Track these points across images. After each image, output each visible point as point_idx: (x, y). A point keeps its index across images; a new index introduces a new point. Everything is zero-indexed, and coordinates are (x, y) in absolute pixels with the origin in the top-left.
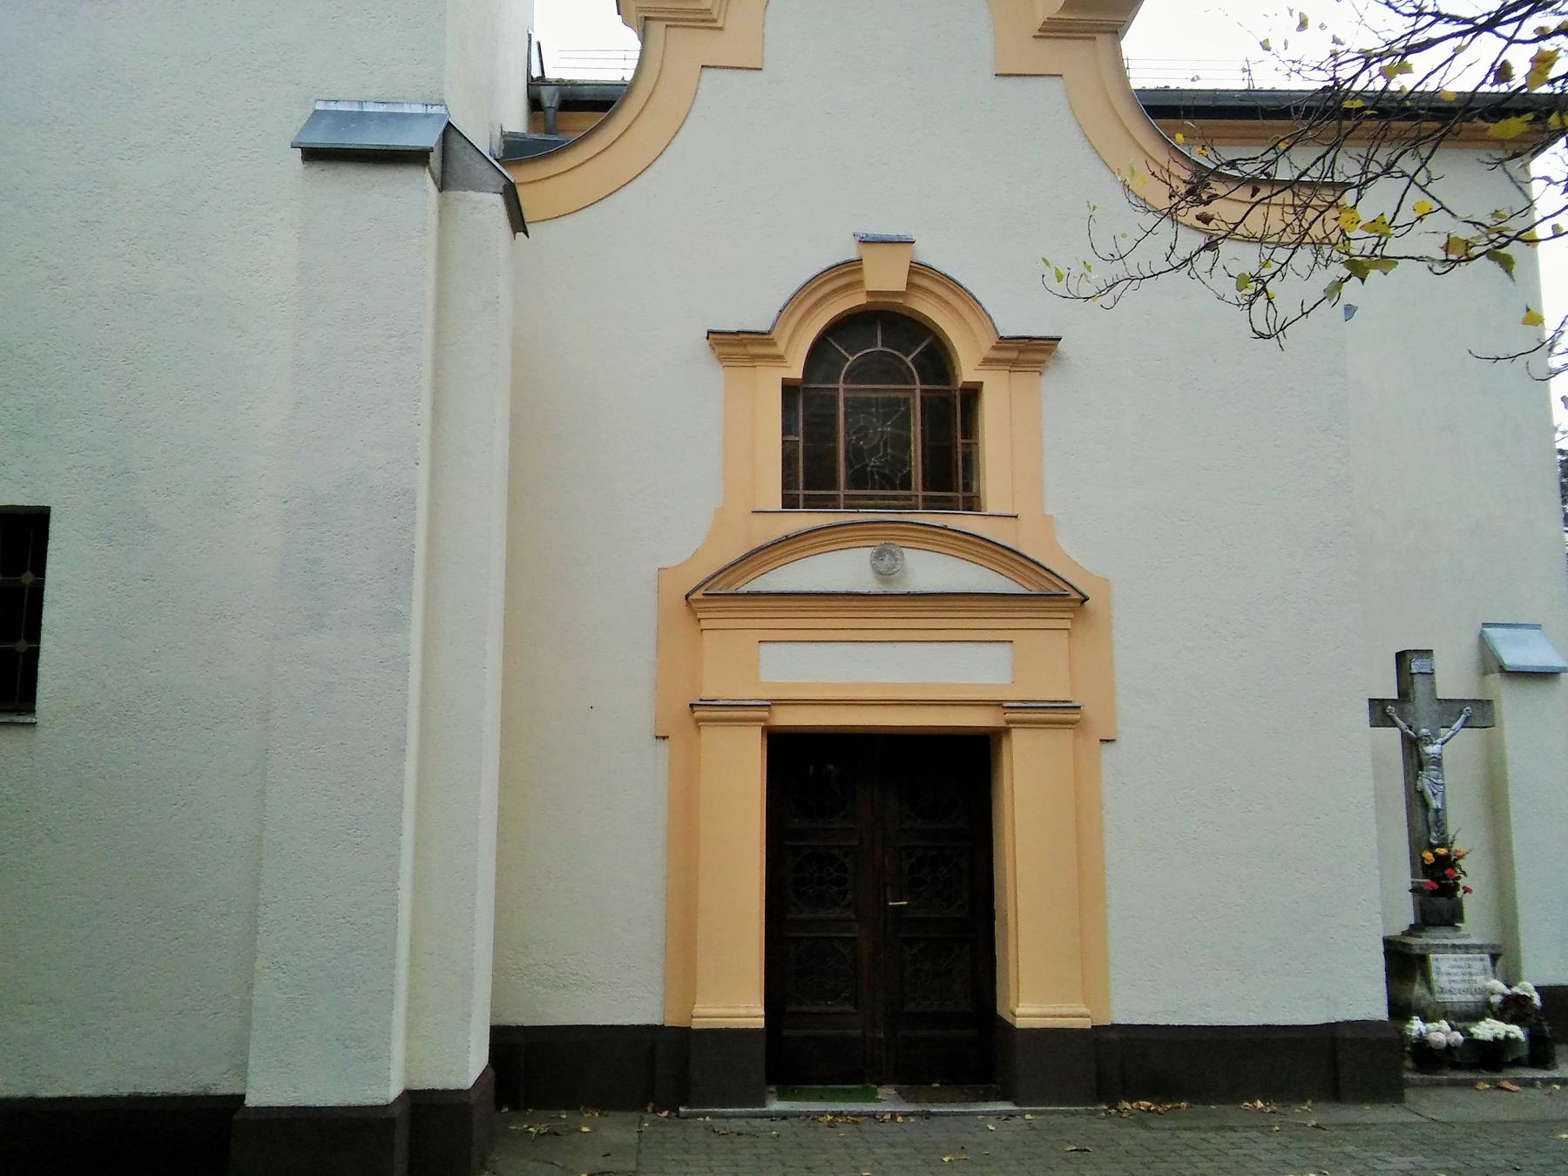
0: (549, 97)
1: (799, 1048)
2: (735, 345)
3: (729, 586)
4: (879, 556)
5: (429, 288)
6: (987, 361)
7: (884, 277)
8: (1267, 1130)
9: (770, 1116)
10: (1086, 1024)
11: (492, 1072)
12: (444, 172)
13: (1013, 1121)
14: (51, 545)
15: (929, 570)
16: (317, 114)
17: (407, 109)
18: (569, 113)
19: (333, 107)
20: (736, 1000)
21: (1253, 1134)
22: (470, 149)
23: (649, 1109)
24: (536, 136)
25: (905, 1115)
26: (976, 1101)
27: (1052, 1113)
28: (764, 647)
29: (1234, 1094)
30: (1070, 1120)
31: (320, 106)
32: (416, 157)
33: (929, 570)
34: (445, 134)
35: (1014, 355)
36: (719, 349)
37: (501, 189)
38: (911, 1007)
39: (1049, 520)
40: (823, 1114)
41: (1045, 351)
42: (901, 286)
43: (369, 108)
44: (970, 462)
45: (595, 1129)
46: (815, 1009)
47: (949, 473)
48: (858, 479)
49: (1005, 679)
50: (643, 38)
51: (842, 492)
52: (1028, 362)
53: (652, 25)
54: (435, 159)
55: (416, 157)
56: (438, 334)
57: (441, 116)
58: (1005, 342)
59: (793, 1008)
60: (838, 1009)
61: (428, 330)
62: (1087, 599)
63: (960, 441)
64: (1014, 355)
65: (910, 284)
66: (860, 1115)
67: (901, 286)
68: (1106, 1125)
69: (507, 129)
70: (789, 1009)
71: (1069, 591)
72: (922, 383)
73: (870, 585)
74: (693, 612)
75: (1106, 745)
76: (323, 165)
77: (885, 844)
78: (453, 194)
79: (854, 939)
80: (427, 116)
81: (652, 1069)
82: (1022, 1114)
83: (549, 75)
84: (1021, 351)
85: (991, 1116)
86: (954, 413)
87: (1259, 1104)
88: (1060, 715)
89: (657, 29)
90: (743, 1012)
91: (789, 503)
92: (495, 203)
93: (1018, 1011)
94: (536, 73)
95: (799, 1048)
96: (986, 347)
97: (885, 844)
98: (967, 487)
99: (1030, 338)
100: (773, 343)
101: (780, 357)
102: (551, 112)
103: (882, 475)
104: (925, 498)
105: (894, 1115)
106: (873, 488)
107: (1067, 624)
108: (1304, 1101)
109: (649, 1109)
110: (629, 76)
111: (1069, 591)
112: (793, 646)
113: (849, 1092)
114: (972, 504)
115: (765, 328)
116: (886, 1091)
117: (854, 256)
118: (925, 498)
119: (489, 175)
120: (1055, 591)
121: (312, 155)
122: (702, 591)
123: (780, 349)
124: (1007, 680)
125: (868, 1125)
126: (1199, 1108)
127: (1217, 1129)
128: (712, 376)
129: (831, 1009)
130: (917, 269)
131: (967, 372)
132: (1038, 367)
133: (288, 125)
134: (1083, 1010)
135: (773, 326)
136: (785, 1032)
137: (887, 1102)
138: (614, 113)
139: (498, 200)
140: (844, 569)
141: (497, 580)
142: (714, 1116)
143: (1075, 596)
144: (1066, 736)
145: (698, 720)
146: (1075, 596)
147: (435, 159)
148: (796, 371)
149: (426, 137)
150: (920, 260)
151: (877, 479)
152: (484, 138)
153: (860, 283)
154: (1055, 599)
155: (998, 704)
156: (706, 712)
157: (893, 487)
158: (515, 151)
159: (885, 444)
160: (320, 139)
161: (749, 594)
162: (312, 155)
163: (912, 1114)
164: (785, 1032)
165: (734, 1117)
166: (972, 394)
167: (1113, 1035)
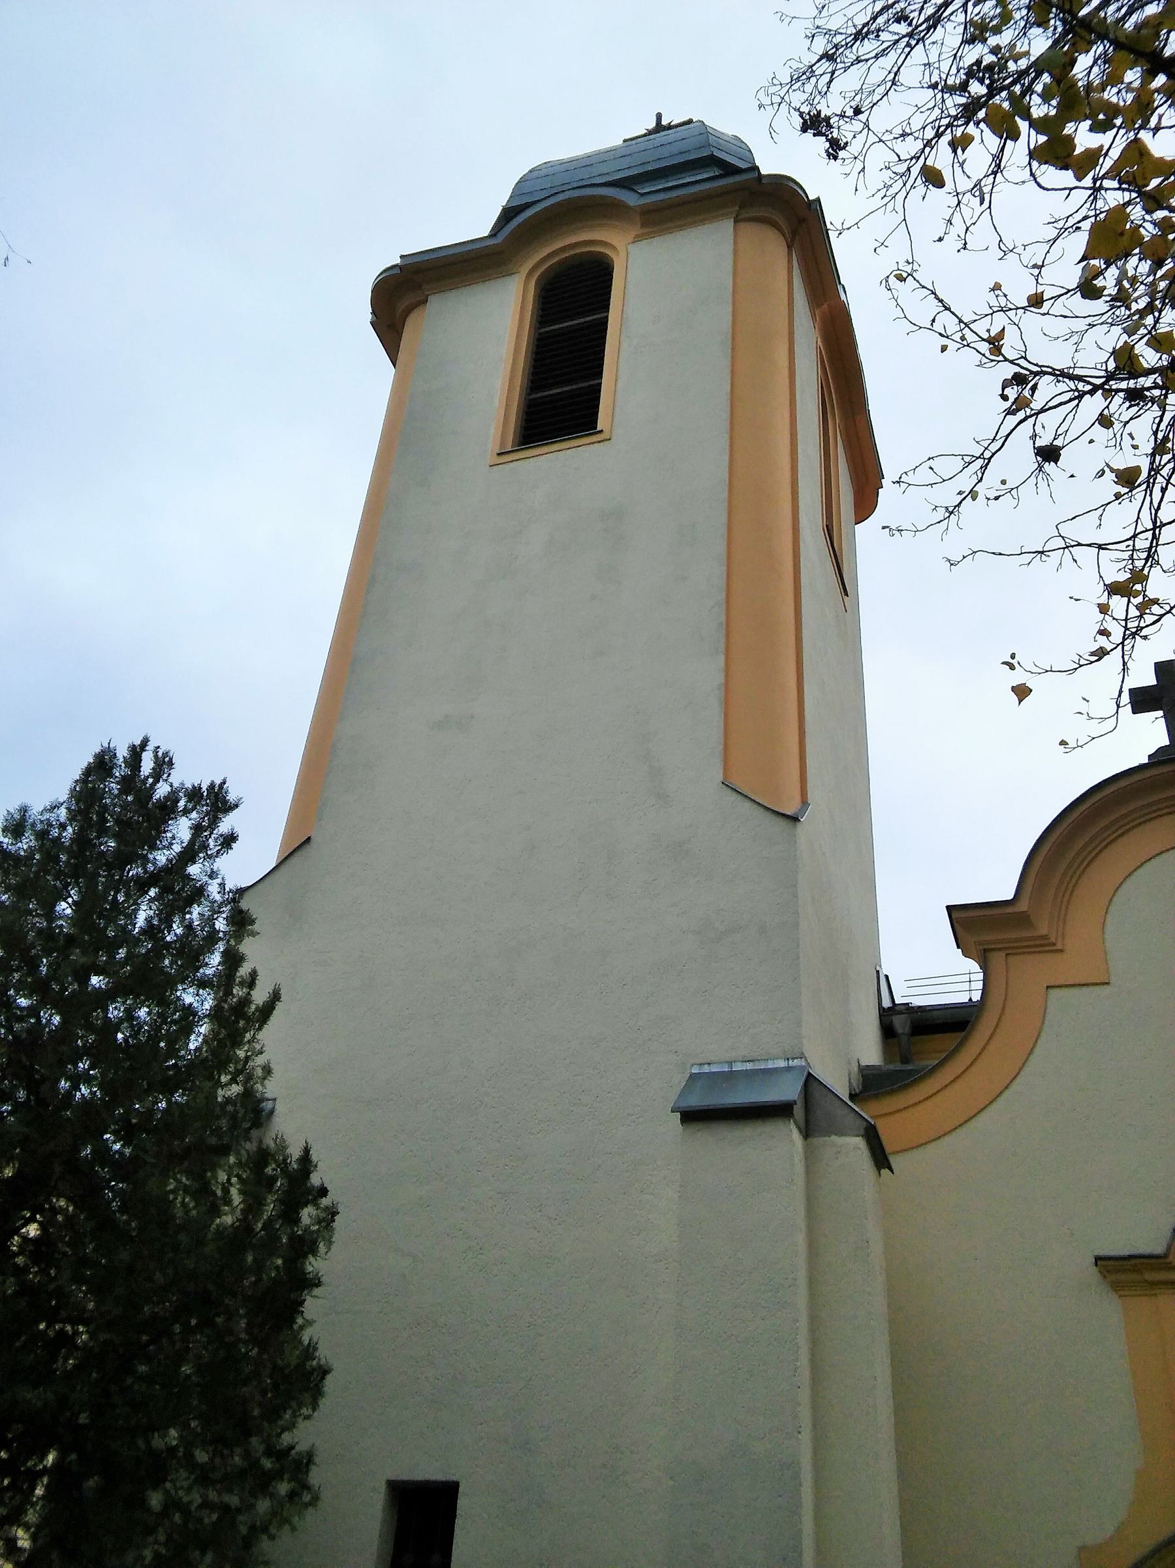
0: (901, 1024)
5: (801, 1239)
12: (807, 1121)
14: (459, 1522)
16: (693, 1077)
17: (770, 1065)
18: (920, 1037)
19: (706, 1069)
22: (825, 1091)
24: (892, 1067)
31: (695, 1070)
32: (779, 1111)
34: (806, 1084)
37: (862, 1132)
43: (738, 1067)
50: (984, 967)
53: (991, 955)
54: (798, 1111)
55: (779, 1111)
56: (812, 1282)
57: (802, 1067)
61: (802, 1282)
69: (863, 1063)
76: (700, 1126)
78: (817, 1141)
80: (789, 1069)
83: (899, 1000)
89: (997, 959)
92: (857, 1144)
94: (886, 1003)
102: (904, 1039)
110: (976, 997)
115: (1159, 1249)
119: (850, 1119)
121: (691, 1117)
133: (666, 1088)
135: (1169, 1248)
138: (969, 1033)
139: (859, 1142)
141: (887, 1464)
147: (798, 1111)
149: (789, 1090)
152: (837, 1079)
158: (872, 1085)
160: (696, 1101)
162: (691, 1117)
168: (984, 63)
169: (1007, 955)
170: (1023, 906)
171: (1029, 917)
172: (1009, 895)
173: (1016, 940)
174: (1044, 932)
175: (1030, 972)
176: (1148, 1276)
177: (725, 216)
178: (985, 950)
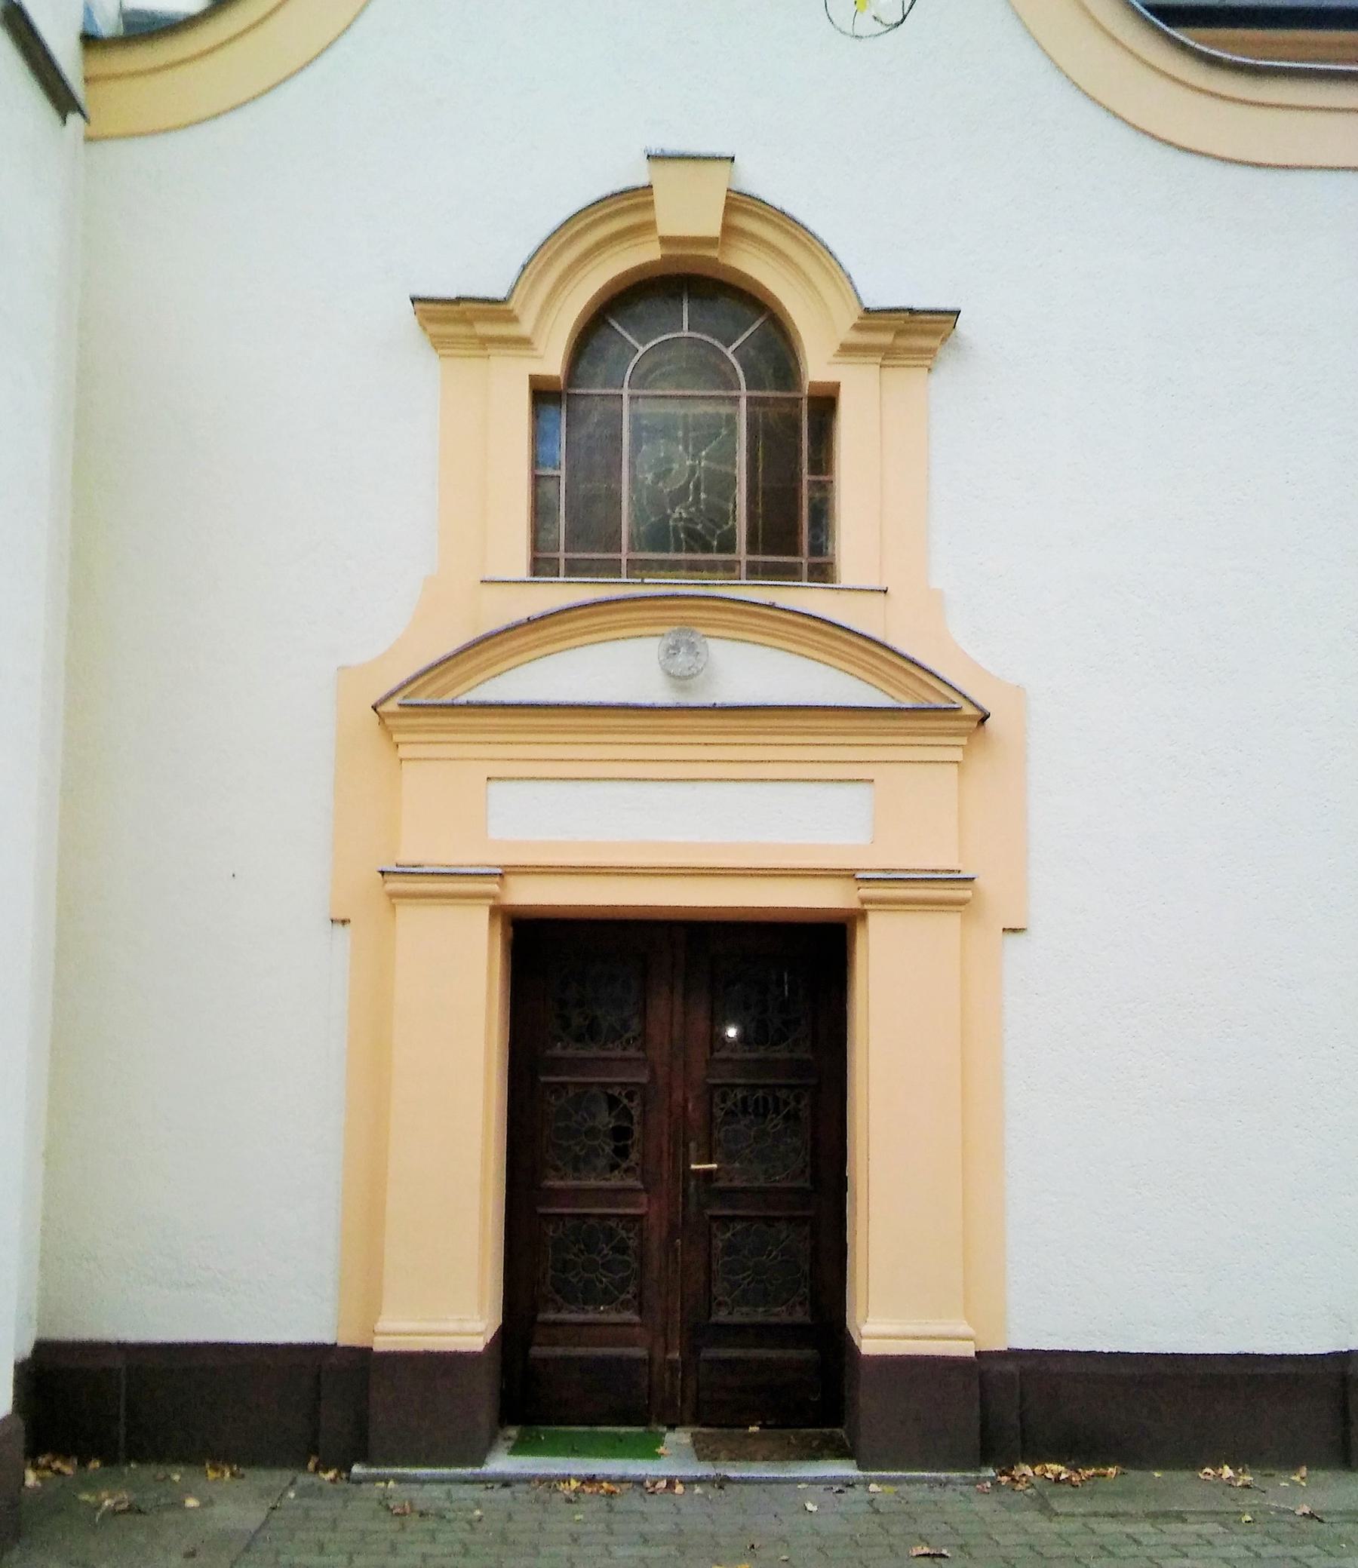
1: (534, 1381)
2: (458, 320)
3: (444, 691)
4: (673, 650)
6: (847, 349)
7: (688, 214)
8: (1228, 1519)
9: (485, 1481)
10: (967, 1350)
11: (20, 1424)
13: (851, 1494)
20: (448, 1301)
21: (1210, 1528)
23: (311, 1465)
25: (689, 1482)
26: (801, 1458)
27: (910, 1481)
28: (494, 786)
29: (1190, 1455)
30: (937, 1493)
33: (748, 670)
35: (886, 339)
36: (434, 328)
38: (721, 1316)
40: (566, 1479)
41: (935, 333)
44: (822, 514)
45: (207, 1503)
46: (581, 1317)
48: (658, 537)
51: (624, 556)
52: (909, 350)
58: (873, 317)
59: (551, 1316)
60: (614, 1317)
63: (806, 477)
64: (886, 339)
65: (728, 229)
66: (622, 1480)
68: (983, 1506)
70: (541, 1317)
71: (960, 702)
73: (660, 694)
74: (388, 732)
75: (1012, 938)
77: (681, 1080)
79: (641, 1216)
81: (317, 1406)
82: (867, 1483)
84: (900, 333)
85: (818, 1488)
86: (797, 437)
87: (1227, 1472)
88: (944, 890)
90: (452, 1326)
91: (541, 566)
93: (865, 1329)
95: (534, 1381)
96: (844, 324)
97: (681, 1080)
100: (512, 318)
101: (524, 342)
103: (692, 534)
105: (671, 1483)
106: (678, 550)
108: (1294, 1467)
109: (311, 1465)
111: (960, 702)
112: (584, 786)
113: (620, 1438)
114: (822, 572)
115: (501, 294)
116: (679, 1438)
117: (642, 181)
122: (398, 699)
123: (525, 328)
125: (629, 1500)
126: (1134, 1475)
127: (1153, 1516)
128: (420, 369)
129: (605, 1318)
130: (738, 203)
131: (817, 366)
134: (964, 1329)
135: (513, 290)
136: (536, 1351)
137: (675, 1456)
140: (622, 666)
142: (400, 1480)
143: (968, 710)
144: (950, 922)
145: (393, 895)
146: (968, 710)
148: (552, 363)
150: (748, 189)
151: (690, 539)
153: (650, 226)
154: (941, 715)
155: (848, 875)
156: (408, 883)
157: (707, 548)
159: (697, 488)
161: (469, 705)
163: (699, 1481)
164: (536, 1351)
165: (427, 1484)
166: (825, 404)
167: (1010, 1367)
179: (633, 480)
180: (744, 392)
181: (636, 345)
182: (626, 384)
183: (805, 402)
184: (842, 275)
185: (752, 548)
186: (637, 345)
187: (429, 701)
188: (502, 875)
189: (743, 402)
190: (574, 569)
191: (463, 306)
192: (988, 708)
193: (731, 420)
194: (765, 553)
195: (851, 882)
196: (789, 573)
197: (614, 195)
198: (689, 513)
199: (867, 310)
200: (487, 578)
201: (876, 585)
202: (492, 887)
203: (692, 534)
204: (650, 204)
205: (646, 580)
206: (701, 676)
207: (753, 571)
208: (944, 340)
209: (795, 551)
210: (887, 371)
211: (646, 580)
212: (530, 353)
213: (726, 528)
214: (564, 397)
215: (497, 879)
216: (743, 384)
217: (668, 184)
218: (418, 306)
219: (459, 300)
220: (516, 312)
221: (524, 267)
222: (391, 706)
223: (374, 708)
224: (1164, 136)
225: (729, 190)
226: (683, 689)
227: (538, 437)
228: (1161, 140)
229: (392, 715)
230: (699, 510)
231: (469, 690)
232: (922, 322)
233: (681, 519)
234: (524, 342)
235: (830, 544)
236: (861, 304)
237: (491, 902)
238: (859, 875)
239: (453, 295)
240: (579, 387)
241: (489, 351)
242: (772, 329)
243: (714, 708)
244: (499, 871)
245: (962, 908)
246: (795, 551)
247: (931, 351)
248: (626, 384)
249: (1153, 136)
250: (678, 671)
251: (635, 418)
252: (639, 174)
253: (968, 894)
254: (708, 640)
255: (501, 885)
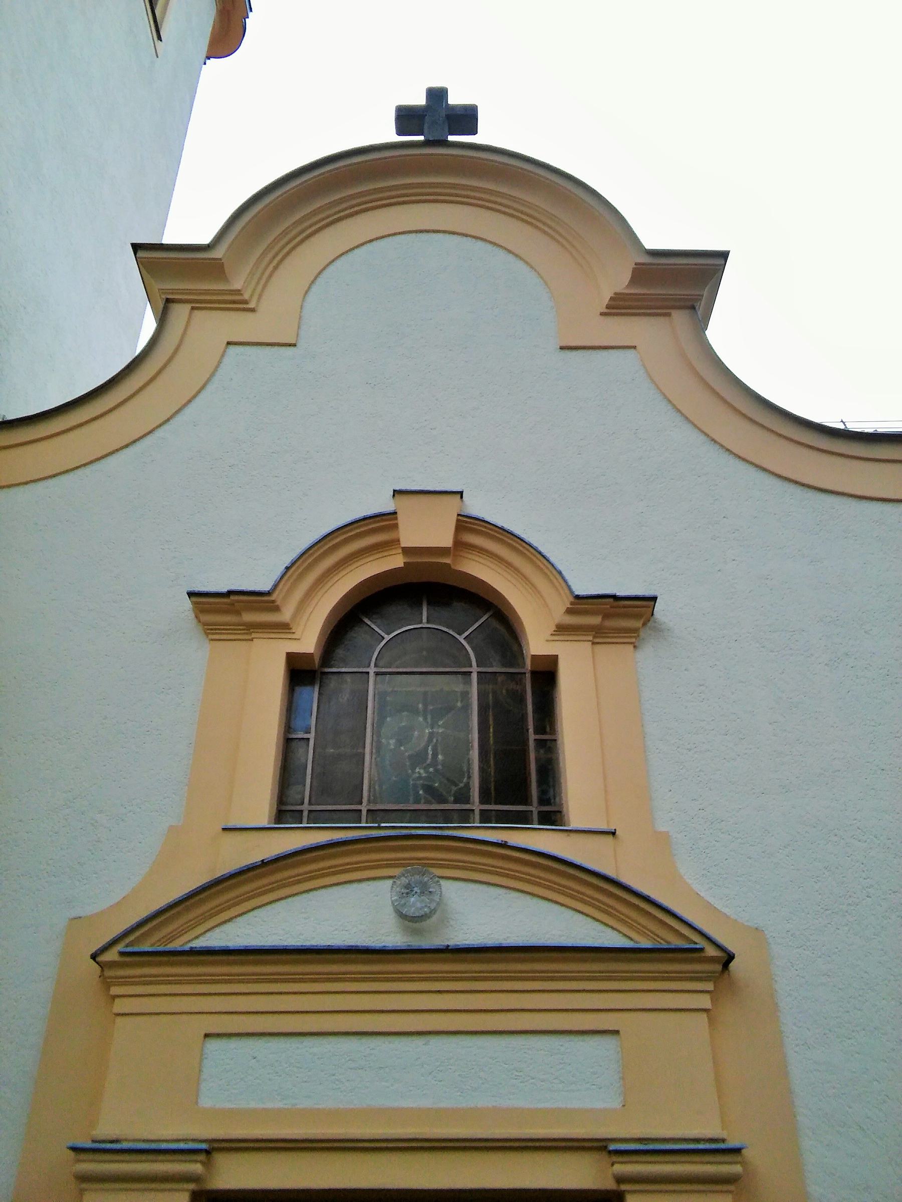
2: (226, 611)
3: (173, 939)
6: (562, 630)
7: (426, 530)
15: (482, 912)
28: (213, 1045)
33: (482, 912)
35: (596, 620)
39: (663, 839)
41: (637, 616)
42: (447, 541)
47: (518, 770)
49: (614, 1102)
50: (162, 319)
62: (731, 957)
63: (532, 737)
64: (596, 620)
65: (459, 545)
67: (447, 541)
71: (701, 943)
72: (460, 634)
73: (392, 936)
74: (106, 983)
84: (606, 616)
86: (523, 705)
89: (180, 312)
91: (285, 813)
96: (558, 609)
98: (544, 800)
99: (615, 597)
101: (284, 627)
103: (429, 789)
104: (482, 812)
107: (705, 1001)
114: (552, 817)
115: (266, 587)
118: (482, 812)
120: (677, 942)
121: (562, 348)
122: (120, 947)
123: (286, 615)
124: (614, 1102)
128: (195, 652)
130: (467, 524)
131: (538, 642)
132: (631, 637)
135: (275, 586)
140: (354, 911)
143: (711, 951)
145: (84, 1178)
146: (711, 951)
148: (308, 641)
154: (686, 959)
161: (193, 952)
162: (562, 348)
166: (546, 676)
168: (642, 622)
169: (193, 308)
170: (218, 253)
171: (221, 266)
172: (205, 238)
173: (207, 292)
174: (237, 285)
175: (210, 329)
176: (249, 617)
177: (454, 107)
178: (168, 301)
179: (378, 747)
180: (475, 669)
181: (380, 634)
182: (372, 664)
183: (528, 676)
184: (554, 572)
185: (485, 797)
186: (383, 634)
187: (150, 949)
188: (210, 1150)
189: (474, 676)
190: (314, 816)
191: (232, 598)
192: (731, 948)
193: (465, 695)
194: (496, 803)
195: (604, 1157)
196: (523, 818)
197: (365, 519)
198: (427, 772)
199: (578, 597)
200: (230, 824)
201: (603, 827)
202: (196, 1168)
203: (429, 789)
204: (396, 526)
205: (383, 825)
206: (434, 919)
207: (486, 817)
208: (644, 624)
209: (526, 801)
210: (598, 648)
211: (383, 825)
212: (290, 636)
213: (462, 785)
214: (318, 675)
215: (202, 1157)
216: (474, 663)
217: (407, 509)
218: (194, 599)
219: (230, 593)
220: (278, 603)
221: (287, 569)
222: (112, 955)
223: (94, 957)
224: (805, 481)
225: (458, 515)
226: (416, 932)
227: (290, 709)
228: (803, 485)
229: (112, 965)
230: (436, 770)
231: (197, 937)
232: (624, 607)
233: (420, 778)
234: (284, 627)
235: (557, 799)
236: (571, 592)
237: (192, 1186)
238: (612, 1147)
239: (224, 590)
240: (331, 667)
241: (254, 635)
242: (495, 624)
243: (447, 950)
244: (204, 1146)
245: (732, 1188)
246: (526, 801)
247: (636, 631)
248: (372, 664)
249: (796, 482)
250: (411, 912)
251: (381, 697)
252: (385, 504)
253: (737, 1169)
254: (443, 882)
255: (207, 1164)
